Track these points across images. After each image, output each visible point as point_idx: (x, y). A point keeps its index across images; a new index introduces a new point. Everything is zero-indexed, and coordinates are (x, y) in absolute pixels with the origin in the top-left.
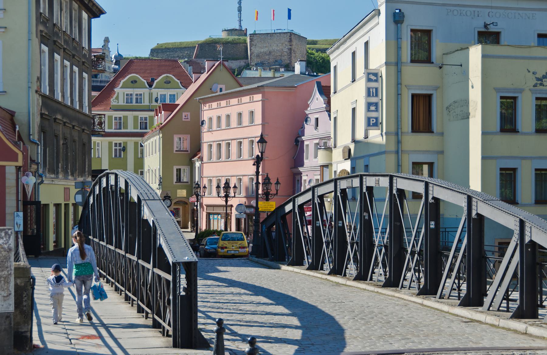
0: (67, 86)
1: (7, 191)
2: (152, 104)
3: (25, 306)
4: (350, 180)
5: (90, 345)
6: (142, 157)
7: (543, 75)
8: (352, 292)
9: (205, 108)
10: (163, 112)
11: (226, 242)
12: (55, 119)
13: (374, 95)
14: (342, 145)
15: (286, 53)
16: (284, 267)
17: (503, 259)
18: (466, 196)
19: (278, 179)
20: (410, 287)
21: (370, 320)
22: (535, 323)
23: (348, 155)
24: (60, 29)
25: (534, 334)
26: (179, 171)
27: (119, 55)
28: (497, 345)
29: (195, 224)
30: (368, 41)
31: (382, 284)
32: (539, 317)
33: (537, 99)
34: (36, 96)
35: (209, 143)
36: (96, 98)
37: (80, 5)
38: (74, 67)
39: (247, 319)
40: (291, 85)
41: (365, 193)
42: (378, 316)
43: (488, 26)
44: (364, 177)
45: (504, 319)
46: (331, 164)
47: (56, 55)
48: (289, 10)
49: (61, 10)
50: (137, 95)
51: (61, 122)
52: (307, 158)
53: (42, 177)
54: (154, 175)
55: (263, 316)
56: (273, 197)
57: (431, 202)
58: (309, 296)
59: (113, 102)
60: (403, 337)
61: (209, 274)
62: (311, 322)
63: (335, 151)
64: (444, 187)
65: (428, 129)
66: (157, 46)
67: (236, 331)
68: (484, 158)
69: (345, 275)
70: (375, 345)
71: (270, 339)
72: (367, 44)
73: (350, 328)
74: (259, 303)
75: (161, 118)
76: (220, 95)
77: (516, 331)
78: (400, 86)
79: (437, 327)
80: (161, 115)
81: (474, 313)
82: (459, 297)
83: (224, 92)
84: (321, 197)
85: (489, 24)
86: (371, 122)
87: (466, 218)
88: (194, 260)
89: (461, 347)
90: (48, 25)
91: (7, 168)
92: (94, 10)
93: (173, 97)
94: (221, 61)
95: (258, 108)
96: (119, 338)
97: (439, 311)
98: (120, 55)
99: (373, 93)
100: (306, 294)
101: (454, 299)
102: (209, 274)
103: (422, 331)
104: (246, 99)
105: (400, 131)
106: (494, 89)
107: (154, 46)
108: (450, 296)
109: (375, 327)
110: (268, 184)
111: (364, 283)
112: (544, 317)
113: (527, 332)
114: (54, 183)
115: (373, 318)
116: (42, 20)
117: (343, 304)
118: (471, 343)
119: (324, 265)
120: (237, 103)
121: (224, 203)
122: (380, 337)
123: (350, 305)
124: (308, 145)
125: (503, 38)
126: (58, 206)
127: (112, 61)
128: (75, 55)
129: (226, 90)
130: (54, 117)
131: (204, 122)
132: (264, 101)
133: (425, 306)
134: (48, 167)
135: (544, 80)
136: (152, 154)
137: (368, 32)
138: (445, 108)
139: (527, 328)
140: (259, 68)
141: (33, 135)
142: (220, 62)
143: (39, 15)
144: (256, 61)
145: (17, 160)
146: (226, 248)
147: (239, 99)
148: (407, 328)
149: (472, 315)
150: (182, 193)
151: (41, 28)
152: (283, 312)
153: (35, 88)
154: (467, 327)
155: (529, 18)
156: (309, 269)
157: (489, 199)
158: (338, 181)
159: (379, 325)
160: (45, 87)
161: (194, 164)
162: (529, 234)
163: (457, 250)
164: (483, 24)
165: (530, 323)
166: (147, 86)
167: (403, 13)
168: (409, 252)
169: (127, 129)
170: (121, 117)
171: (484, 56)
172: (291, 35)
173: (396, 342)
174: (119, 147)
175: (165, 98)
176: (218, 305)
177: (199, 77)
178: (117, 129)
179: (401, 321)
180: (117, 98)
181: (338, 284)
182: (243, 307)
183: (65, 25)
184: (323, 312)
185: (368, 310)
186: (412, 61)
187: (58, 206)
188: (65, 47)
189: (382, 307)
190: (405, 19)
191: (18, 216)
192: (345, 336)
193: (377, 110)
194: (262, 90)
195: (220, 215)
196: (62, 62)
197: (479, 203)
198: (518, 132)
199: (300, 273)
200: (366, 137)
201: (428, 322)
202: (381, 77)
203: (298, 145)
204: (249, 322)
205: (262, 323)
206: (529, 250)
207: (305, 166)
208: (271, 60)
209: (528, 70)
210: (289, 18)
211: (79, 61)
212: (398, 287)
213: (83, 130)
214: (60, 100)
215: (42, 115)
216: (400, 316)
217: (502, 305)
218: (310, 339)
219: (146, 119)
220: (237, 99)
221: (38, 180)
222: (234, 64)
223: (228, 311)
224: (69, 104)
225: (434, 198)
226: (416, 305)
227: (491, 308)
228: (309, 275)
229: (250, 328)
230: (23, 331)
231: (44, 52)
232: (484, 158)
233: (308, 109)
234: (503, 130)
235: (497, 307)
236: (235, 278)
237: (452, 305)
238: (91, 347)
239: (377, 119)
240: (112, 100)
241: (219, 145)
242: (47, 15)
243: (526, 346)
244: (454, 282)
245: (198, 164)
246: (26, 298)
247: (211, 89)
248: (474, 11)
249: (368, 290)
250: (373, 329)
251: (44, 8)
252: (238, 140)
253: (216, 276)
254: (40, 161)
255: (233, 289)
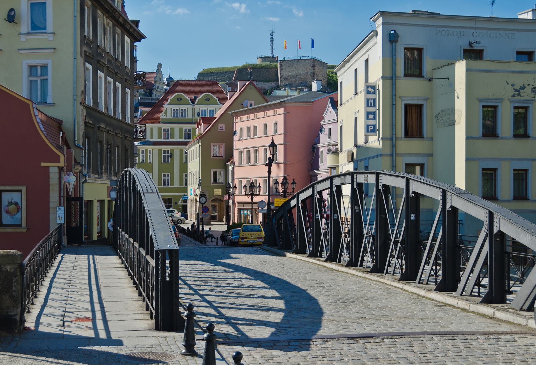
0: (110, 99)
1: (51, 188)
2: (194, 118)
3: (15, 291)
4: (343, 177)
5: (79, 327)
6: (186, 163)
7: (521, 87)
8: (342, 277)
9: (237, 121)
10: (202, 124)
11: (246, 233)
12: (99, 127)
13: (372, 106)
14: (347, 149)
15: (310, 76)
16: (289, 255)
17: (474, 248)
18: (441, 191)
19: (294, 180)
20: (394, 273)
21: (351, 304)
22: (502, 307)
23: (351, 158)
24: (104, 50)
25: (501, 319)
26: (215, 173)
27: (171, 78)
28: (464, 329)
29: (228, 219)
30: (367, 59)
31: (369, 270)
32: (507, 302)
33: (515, 107)
34: (81, 107)
35: (240, 150)
36: (148, 113)
37: (123, 30)
38: (100, 74)
39: (239, 301)
40: (308, 100)
41: (355, 189)
42: (359, 300)
43: (472, 45)
44: (355, 175)
45: (474, 304)
46: (338, 166)
47: (99, 72)
48: (313, 41)
49: (105, 34)
50: (182, 110)
51: (105, 130)
52: (322, 163)
53: (86, 177)
54: (195, 177)
55: (253, 300)
56: (289, 195)
57: (411, 196)
58: (302, 281)
59: (162, 116)
60: (377, 321)
61: (221, 261)
62: (295, 306)
63: (341, 155)
64: (422, 182)
65: (419, 135)
66: (203, 71)
67: (224, 313)
68: (467, 160)
69: (339, 262)
70: (348, 328)
71: (252, 322)
72: (367, 61)
73: (330, 311)
74: (255, 287)
75: (201, 129)
76: (249, 109)
77: (484, 316)
78: (394, 97)
79: (411, 311)
80: (201, 127)
81: (447, 298)
82: (436, 282)
83: (253, 107)
84: (320, 193)
85: (473, 43)
86: (370, 129)
87: (441, 211)
88: (175, 248)
89: (429, 331)
90: (92, 46)
91: (51, 169)
92: (135, 35)
93: (212, 112)
94: (250, 81)
95: (280, 120)
96: (110, 321)
97: (416, 296)
98: (171, 77)
99: (371, 103)
100: (300, 279)
101: (432, 285)
102: (221, 261)
103: (396, 314)
104: (270, 112)
105: (394, 136)
106: (478, 99)
107: (200, 70)
108: (428, 281)
109: (353, 310)
110: (286, 183)
111: (354, 269)
112: (512, 302)
113: (495, 317)
114: (97, 182)
115: (354, 302)
116: (86, 42)
117: (331, 288)
118: (439, 327)
119: (323, 253)
120: (263, 116)
121: (250, 200)
122: (355, 321)
123: (337, 289)
124: (323, 151)
125: (486, 55)
126: (101, 202)
127: (164, 83)
128: (118, 73)
129: (255, 105)
130: (98, 126)
131: (236, 132)
132: (286, 115)
133: (405, 290)
134: (92, 168)
135: (521, 91)
136: (196, 159)
137: (368, 51)
138: (434, 116)
139: (494, 312)
140: (286, 88)
141: (78, 140)
142: (250, 82)
143: (83, 38)
144: (284, 82)
145: (59, 162)
146: (246, 238)
147: (265, 113)
148: (383, 312)
149: (446, 300)
150: (218, 192)
151: (85, 48)
152: (274, 295)
153: (80, 100)
154: (440, 311)
155: (508, 37)
156: (309, 256)
157: (463, 193)
158: (334, 179)
159: (358, 308)
160: (89, 100)
161: (228, 168)
162: (498, 225)
163: (434, 239)
164: (468, 43)
165: (497, 308)
166: (191, 103)
167: (397, 33)
168: (393, 241)
169: (174, 139)
170: (169, 129)
171: (468, 70)
172: (314, 61)
173: (368, 325)
174: (167, 153)
175: (206, 113)
176: (218, 288)
177: (233, 95)
178: (165, 139)
179: (379, 305)
180: (166, 113)
181: (332, 270)
182: (239, 291)
183: (108, 47)
184: (310, 296)
185: (351, 294)
186: (405, 76)
187: (101, 202)
188: (109, 66)
189: (365, 291)
190: (399, 39)
191: (60, 210)
192: (323, 319)
193: (374, 118)
194: (284, 105)
195: (249, 211)
196: (106, 79)
197: (453, 196)
198: (498, 137)
199: (301, 260)
200: (366, 142)
201: (404, 305)
202: (378, 89)
203: (314, 152)
204: (240, 305)
205: (251, 306)
206: (498, 239)
207: (320, 169)
208: (297, 82)
209: (507, 82)
210: (313, 46)
211: (121, 78)
212: (383, 273)
213: (126, 137)
214: (103, 111)
215: (86, 123)
216: (379, 300)
217: (474, 290)
218: (289, 322)
219: (189, 130)
220: (263, 113)
221: (82, 179)
222: (267, 86)
223: (225, 294)
224: (112, 115)
225: (414, 192)
226: (396, 289)
227: (464, 293)
228: (309, 262)
229: (238, 311)
230: (12, 314)
231: (88, 69)
232: (468, 160)
233: (323, 121)
234: (485, 135)
235: (469, 293)
236: (242, 265)
237: (429, 290)
238: (80, 329)
239: (374, 126)
240: (161, 114)
241: (249, 152)
242: (91, 38)
243: (492, 330)
244: (432, 269)
245: (231, 168)
246: (15, 283)
247: (242, 105)
248: (460, 32)
249: (357, 276)
250: (351, 312)
251: (89, 32)
252: (264, 147)
253: (226, 262)
254: (84, 163)
255: (237, 275)
